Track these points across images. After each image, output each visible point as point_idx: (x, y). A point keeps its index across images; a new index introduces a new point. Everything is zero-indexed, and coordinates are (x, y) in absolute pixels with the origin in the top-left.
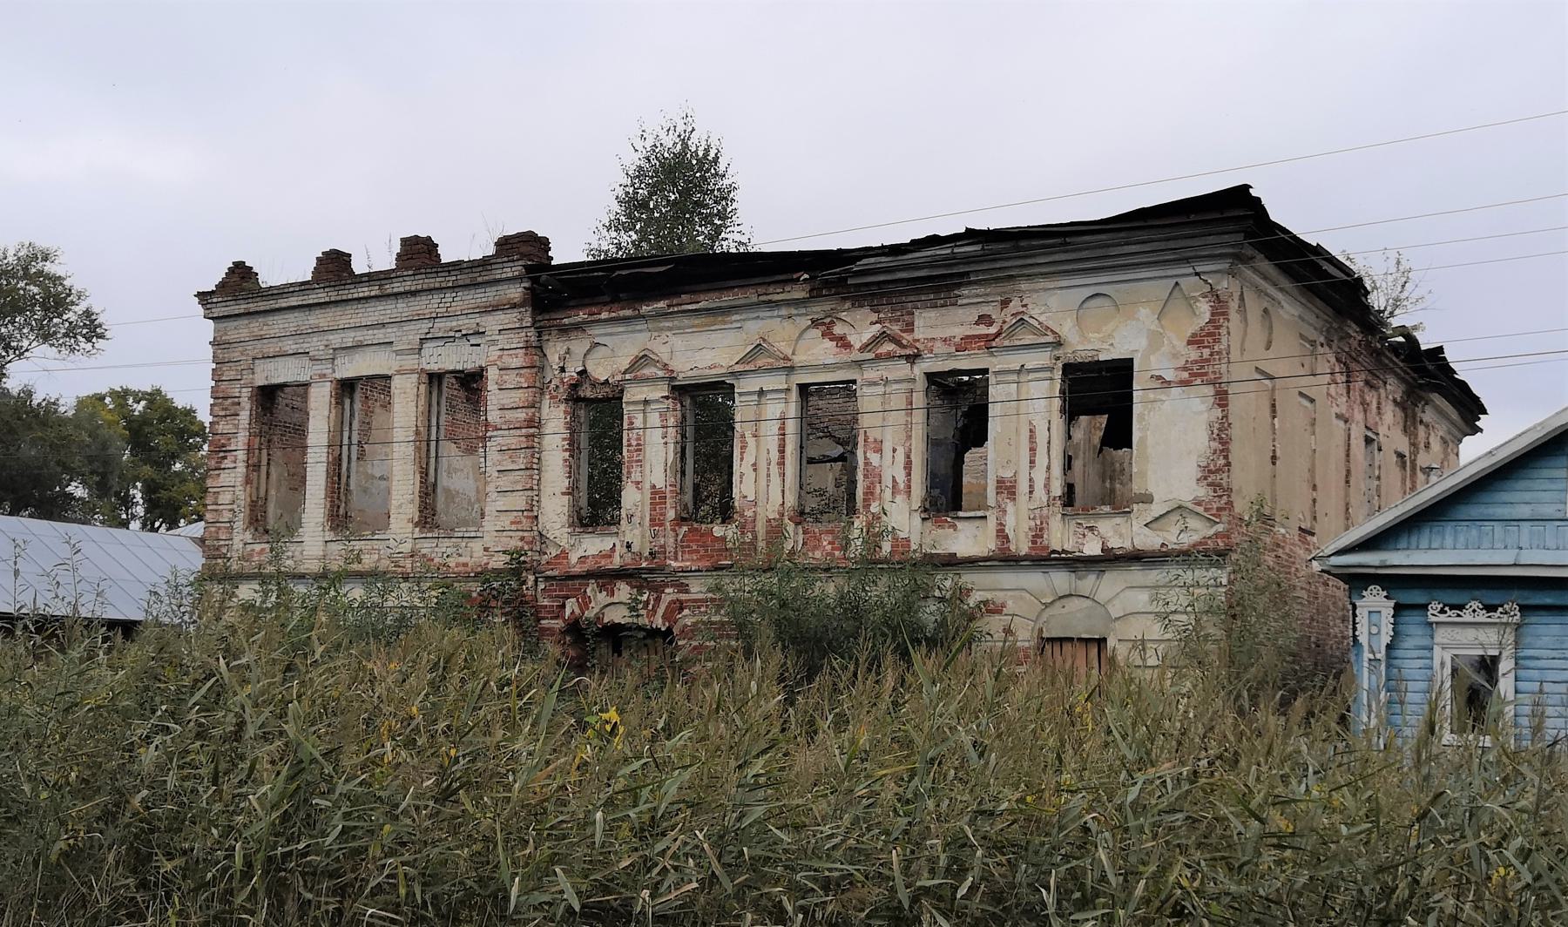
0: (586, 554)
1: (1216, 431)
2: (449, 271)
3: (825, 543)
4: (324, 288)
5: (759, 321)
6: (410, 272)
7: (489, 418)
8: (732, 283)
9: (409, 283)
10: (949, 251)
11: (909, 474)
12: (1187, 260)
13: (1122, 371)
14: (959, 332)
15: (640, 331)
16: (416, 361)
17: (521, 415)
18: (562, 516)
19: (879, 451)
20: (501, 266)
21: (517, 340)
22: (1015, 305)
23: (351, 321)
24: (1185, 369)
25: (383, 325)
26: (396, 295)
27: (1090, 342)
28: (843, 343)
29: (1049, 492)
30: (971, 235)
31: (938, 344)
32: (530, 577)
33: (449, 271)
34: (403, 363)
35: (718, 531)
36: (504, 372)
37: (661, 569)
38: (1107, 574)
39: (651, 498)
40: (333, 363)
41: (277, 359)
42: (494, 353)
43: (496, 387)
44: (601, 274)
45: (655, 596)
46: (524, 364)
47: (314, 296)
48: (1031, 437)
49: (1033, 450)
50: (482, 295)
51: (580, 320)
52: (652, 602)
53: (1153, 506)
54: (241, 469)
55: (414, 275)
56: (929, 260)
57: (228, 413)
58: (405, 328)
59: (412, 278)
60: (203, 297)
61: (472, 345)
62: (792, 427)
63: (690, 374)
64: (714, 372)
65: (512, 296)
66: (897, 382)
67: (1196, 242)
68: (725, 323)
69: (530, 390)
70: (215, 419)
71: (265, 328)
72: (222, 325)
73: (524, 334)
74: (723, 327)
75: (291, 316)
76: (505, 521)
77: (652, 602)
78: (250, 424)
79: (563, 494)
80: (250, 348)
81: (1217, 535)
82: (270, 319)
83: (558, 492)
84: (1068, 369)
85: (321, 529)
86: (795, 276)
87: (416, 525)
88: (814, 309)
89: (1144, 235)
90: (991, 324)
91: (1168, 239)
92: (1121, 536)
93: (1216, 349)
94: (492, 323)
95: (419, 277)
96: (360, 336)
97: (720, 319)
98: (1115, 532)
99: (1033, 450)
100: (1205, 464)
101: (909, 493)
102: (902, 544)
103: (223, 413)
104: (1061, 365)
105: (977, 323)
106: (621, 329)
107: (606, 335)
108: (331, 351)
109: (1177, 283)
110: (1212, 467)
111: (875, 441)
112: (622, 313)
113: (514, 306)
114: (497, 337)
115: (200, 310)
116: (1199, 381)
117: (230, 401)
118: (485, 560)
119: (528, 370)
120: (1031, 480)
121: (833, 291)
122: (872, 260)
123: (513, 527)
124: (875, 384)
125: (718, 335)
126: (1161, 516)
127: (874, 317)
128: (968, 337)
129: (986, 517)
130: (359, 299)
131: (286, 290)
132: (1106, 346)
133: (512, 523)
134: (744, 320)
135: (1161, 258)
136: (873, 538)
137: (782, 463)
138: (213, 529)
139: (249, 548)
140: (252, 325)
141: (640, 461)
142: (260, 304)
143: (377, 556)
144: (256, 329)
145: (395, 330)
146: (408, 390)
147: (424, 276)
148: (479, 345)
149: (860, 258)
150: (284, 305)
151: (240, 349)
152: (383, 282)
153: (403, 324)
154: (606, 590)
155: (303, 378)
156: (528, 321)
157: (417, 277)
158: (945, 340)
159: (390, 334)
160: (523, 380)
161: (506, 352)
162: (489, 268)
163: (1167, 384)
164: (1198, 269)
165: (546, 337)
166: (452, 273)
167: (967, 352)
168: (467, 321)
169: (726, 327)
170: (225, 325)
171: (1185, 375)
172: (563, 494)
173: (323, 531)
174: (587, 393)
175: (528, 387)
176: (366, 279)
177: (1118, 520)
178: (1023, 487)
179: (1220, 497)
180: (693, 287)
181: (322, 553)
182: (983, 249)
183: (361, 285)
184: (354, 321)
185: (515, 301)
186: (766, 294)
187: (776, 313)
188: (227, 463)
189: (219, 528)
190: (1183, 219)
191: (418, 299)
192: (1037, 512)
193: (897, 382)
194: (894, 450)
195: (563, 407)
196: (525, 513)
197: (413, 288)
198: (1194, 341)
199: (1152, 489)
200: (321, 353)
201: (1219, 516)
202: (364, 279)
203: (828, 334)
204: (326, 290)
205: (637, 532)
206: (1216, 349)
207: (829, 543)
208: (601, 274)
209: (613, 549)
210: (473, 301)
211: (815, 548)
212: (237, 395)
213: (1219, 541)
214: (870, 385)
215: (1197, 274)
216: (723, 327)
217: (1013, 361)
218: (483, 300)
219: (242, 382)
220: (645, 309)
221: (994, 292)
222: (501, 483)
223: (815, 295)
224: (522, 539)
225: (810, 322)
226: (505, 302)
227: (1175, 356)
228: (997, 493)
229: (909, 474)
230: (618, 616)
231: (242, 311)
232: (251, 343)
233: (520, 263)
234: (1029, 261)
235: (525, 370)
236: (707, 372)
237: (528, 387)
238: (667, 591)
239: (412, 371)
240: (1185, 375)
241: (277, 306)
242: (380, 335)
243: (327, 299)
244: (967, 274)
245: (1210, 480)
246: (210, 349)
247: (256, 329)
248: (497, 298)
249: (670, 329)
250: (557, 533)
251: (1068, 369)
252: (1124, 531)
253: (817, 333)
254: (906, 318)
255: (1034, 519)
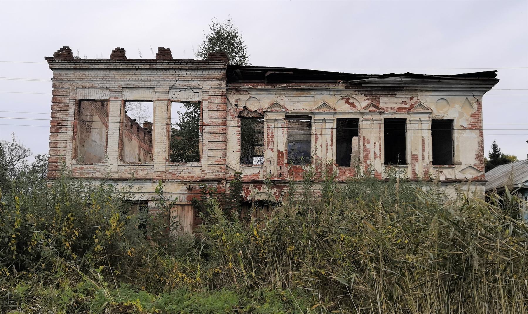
0: (247, 174)
1: (480, 144)
2: (187, 63)
3: (347, 174)
4: (120, 63)
5: (321, 95)
6: (167, 61)
7: (204, 121)
8: (310, 81)
9: (165, 65)
10: (400, 79)
11: (380, 151)
12: (472, 91)
13: (449, 123)
14: (396, 106)
15: (272, 94)
16: (167, 96)
17: (220, 121)
18: (237, 159)
19: (369, 143)
20: (213, 64)
21: (218, 92)
22: (415, 99)
23: (133, 77)
24: (470, 124)
25: (150, 80)
26: (157, 69)
27: (440, 113)
28: (353, 105)
29: (429, 160)
30: (408, 75)
31: (389, 109)
32: (224, 182)
33: (187, 63)
34: (159, 96)
35: (307, 168)
36: (211, 104)
37: (284, 181)
38: (448, 187)
39: (278, 155)
40: (122, 93)
41: (90, 89)
42: (206, 97)
43: (207, 109)
44: (260, 71)
45: (279, 190)
46: (221, 102)
47: (114, 65)
48: (423, 142)
49: (424, 146)
50: (202, 74)
51: (248, 88)
52: (278, 193)
53: (462, 166)
54: (70, 133)
55: (169, 62)
56: (393, 81)
57: (62, 109)
58: (161, 83)
59: (168, 63)
60: (49, 59)
61: (194, 92)
62: (335, 131)
63: (294, 111)
64: (304, 111)
65: (216, 76)
66: (376, 120)
67: (479, 86)
68: (308, 94)
69: (224, 112)
70: (54, 112)
71: (83, 76)
72: (58, 72)
73: (221, 90)
74: (306, 96)
75: (99, 72)
76: (213, 161)
77: (278, 193)
78: (74, 115)
79: (238, 152)
80: (75, 83)
81: (481, 175)
82: (87, 72)
83: (235, 151)
84: (433, 121)
85: (117, 160)
86: (338, 81)
87: (167, 160)
88: (344, 93)
89: (463, 82)
90: (406, 104)
91: (470, 84)
92: (451, 175)
93: (479, 119)
94: (206, 85)
95: (171, 63)
96: (137, 83)
97: (306, 93)
98: (449, 173)
99: (424, 146)
100: (477, 154)
101: (380, 158)
102: (378, 175)
103: (60, 109)
104: (431, 120)
105: (402, 104)
106: (264, 93)
107: (256, 94)
108: (122, 88)
109: (467, 98)
110: (479, 155)
111: (368, 139)
112: (267, 87)
113: (217, 79)
114: (208, 91)
115: (48, 65)
116: (474, 128)
117: (62, 104)
118: (203, 175)
119: (222, 104)
120: (423, 156)
121: (354, 88)
122: (373, 79)
123: (217, 163)
124: (368, 120)
125: (304, 98)
126: (464, 169)
127: (366, 98)
128: (399, 108)
129: (407, 167)
130: (137, 69)
131: (99, 61)
132: (445, 115)
133: (216, 162)
134: (315, 94)
135: (452, 90)
136: (368, 171)
137: (332, 145)
138: (55, 158)
139: (74, 167)
140: (76, 74)
141: (273, 141)
142: (82, 66)
143: (146, 172)
144: (78, 76)
145: (156, 83)
146: (162, 107)
147: (173, 63)
148: (198, 93)
149: (368, 78)
150: (97, 67)
151: (69, 83)
152: (152, 64)
153: (160, 81)
154: (258, 188)
155: (105, 98)
156: (224, 85)
157: (169, 63)
158: (391, 108)
159: (154, 84)
160: (221, 108)
161: (212, 97)
162: (207, 64)
163: (464, 128)
164: (474, 94)
165: (230, 93)
166: (188, 64)
167: (400, 113)
168: (193, 83)
169: (308, 96)
170: (60, 72)
171: (470, 126)
172: (238, 152)
173: (118, 161)
174: (245, 114)
175: (223, 111)
176: (144, 61)
177: (450, 170)
178: (420, 158)
179: (482, 164)
180: (254, 81)
181: (117, 170)
182: (412, 80)
183: (140, 63)
184: (134, 77)
185: (218, 78)
186: (328, 86)
187: (329, 93)
188: (62, 130)
189: (58, 158)
190: (477, 78)
191: (168, 72)
192: (426, 166)
193: (376, 120)
194: (375, 143)
195: (237, 119)
196: (222, 158)
197: (168, 68)
198: (473, 116)
199: (461, 161)
200: (116, 89)
201: (481, 170)
202: (142, 61)
203: (347, 102)
204: (121, 64)
205: (272, 167)
206: (479, 119)
207: (349, 174)
208: (260, 71)
209: (259, 173)
210: (196, 76)
211: (343, 175)
212: (68, 102)
213: (482, 177)
214: (366, 121)
215: (473, 96)
216: (306, 96)
217: (417, 117)
218: (201, 76)
219: (70, 97)
220: (278, 86)
221: (409, 94)
222: (211, 146)
223: (347, 88)
224: (221, 168)
225: (341, 97)
226: (213, 77)
227: (467, 120)
228: (412, 159)
229: (380, 151)
230: (263, 197)
231: (72, 67)
232: (76, 81)
233: (223, 63)
234: (425, 86)
235: (221, 104)
236: (301, 111)
237: (223, 111)
238: (284, 189)
239: (165, 100)
240: (470, 126)
241: (93, 67)
242: (148, 84)
243: (218, 67)
244: (403, 87)
245: (479, 159)
246: (51, 83)
247: (78, 76)
248: (208, 76)
249: (284, 94)
250: (235, 166)
251: (433, 121)
252: (452, 173)
253: (343, 101)
254: (377, 99)
255: (425, 168)
